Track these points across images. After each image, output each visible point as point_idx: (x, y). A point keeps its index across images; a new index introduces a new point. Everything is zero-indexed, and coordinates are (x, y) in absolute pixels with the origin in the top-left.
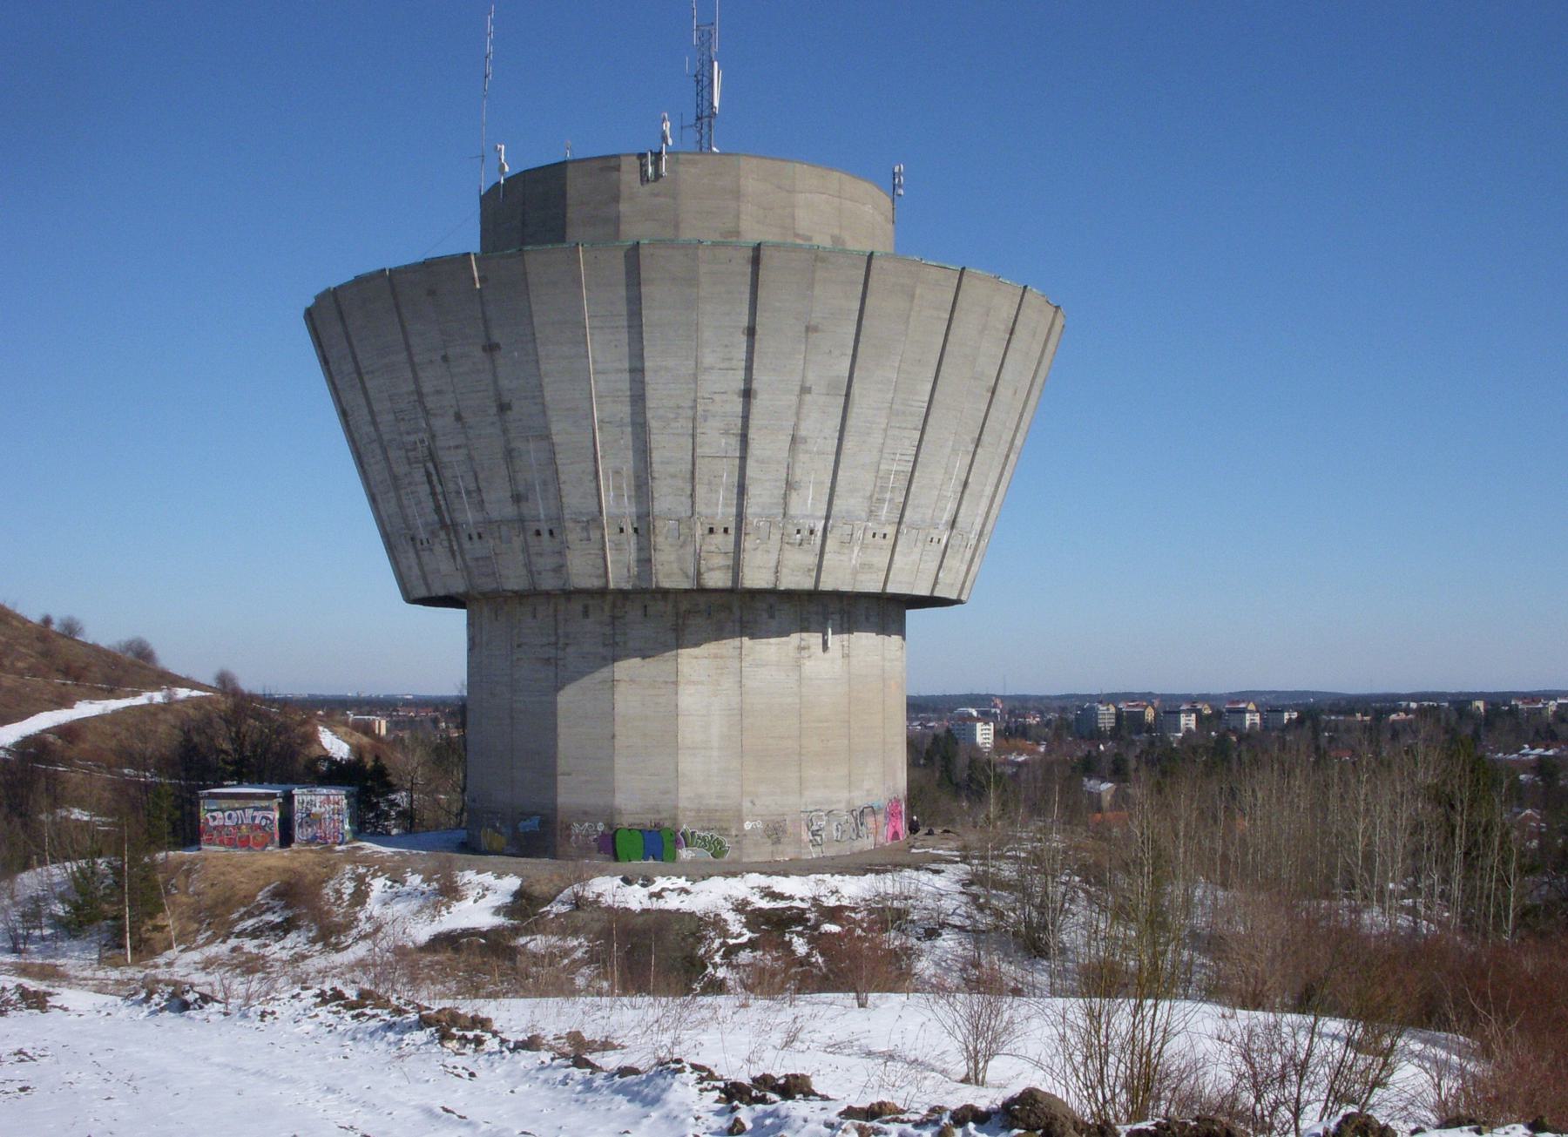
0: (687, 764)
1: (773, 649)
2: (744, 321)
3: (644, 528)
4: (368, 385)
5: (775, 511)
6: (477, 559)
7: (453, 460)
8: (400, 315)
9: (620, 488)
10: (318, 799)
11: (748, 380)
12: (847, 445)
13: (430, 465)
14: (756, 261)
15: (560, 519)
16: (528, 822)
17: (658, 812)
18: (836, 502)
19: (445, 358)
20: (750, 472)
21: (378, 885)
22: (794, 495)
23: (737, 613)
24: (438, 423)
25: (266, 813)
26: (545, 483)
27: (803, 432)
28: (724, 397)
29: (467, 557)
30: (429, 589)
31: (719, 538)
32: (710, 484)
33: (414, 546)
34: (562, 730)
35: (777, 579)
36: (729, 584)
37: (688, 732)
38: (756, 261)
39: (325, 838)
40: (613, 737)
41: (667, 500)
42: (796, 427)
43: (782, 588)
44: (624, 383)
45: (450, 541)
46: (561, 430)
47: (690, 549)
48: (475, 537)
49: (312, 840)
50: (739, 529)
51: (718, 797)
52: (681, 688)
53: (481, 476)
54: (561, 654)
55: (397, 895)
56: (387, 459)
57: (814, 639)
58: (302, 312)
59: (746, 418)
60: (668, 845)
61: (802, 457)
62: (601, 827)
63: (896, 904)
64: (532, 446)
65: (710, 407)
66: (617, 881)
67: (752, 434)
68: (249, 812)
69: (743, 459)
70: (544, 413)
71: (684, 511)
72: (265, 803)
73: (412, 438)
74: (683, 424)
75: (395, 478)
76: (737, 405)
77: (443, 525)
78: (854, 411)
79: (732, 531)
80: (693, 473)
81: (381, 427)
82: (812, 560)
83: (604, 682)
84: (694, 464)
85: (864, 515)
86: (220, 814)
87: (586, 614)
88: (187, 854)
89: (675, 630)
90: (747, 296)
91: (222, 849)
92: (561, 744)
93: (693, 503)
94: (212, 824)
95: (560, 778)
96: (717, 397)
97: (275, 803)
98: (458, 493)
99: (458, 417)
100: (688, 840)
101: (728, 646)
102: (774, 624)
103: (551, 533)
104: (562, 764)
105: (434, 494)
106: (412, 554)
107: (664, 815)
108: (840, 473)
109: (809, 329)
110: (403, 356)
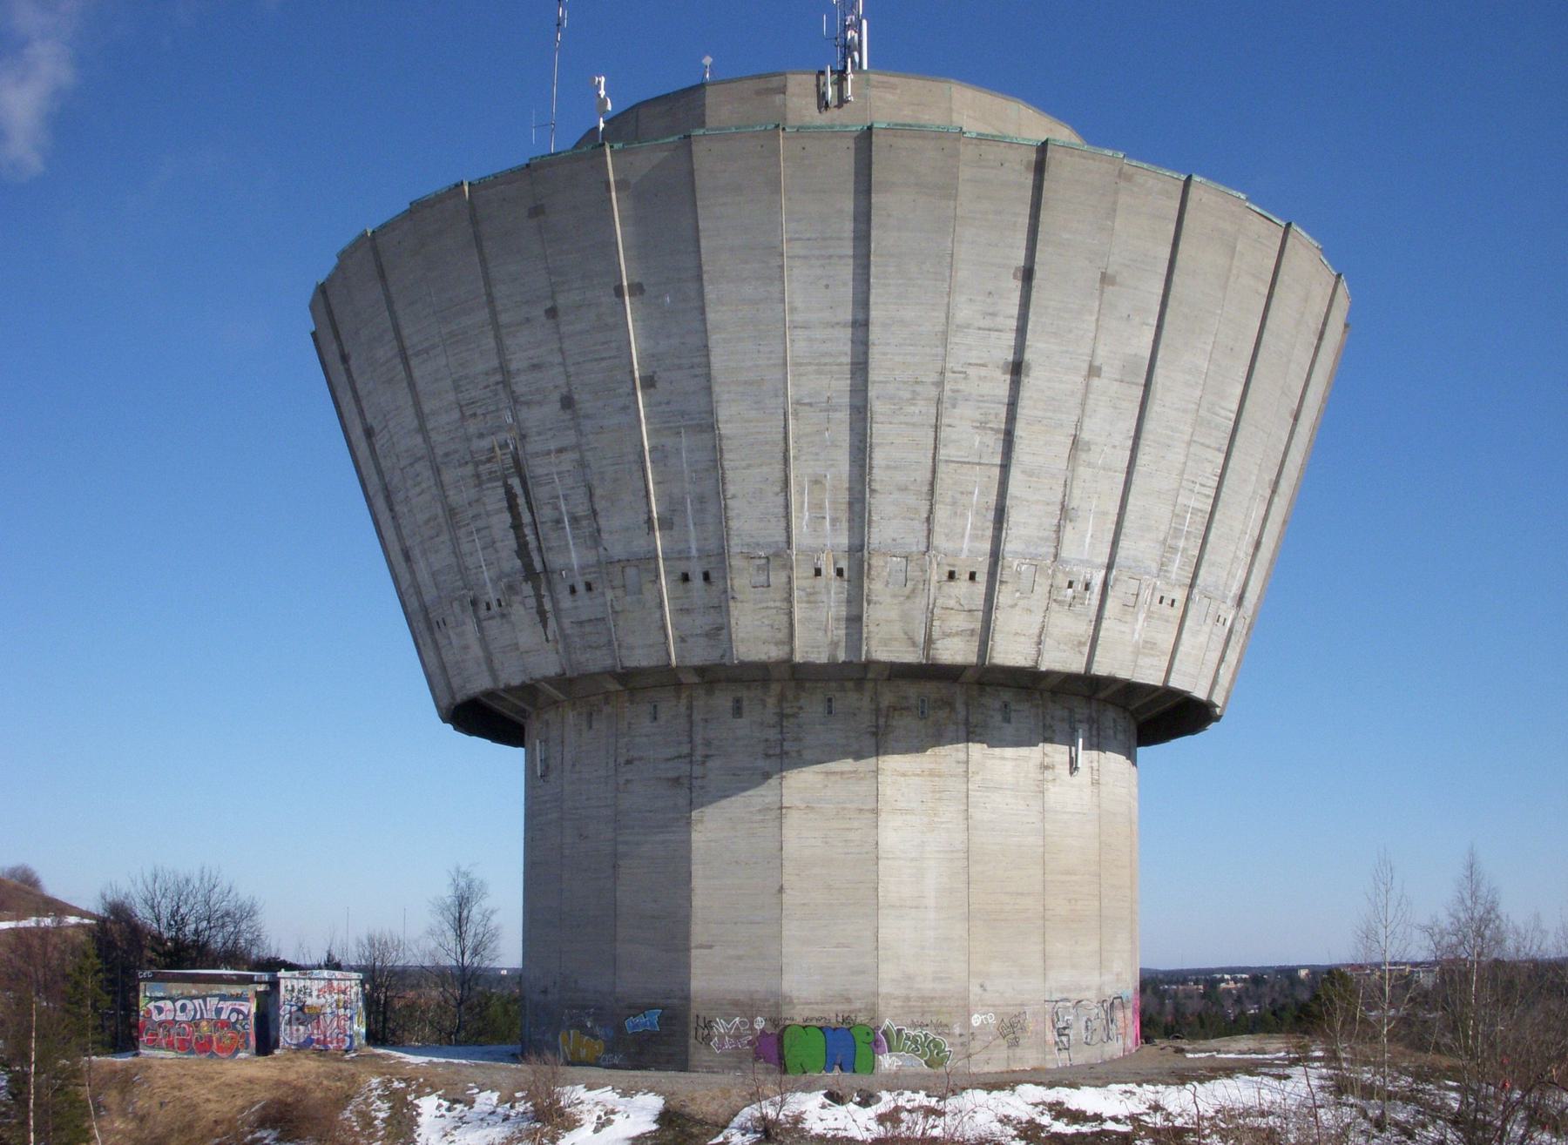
0: (890, 928)
1: (1009, 765)
2: (1019, 258)
3: (856, 567)
4: (416, 374)
5: (1043, 550)
6: (581, 623)
7: (553, 475)
8: (481, 252)
9: (821, 507)
10: (315, 986)
11: (1020, 347)
12: (1142, 459)
13: (515, 482)
14: (1040, 168)
15: (722, 555)
16: (640, 1019)
17: (848, 1000)
18: (1123, 543)
19: (552, 313)
20: (1013, 489)
21: (429, 1106)
22: (1069, 526)
23: (960, 707)
24: (532, 417)
25: (238, 1005)
26: (701, 499)
27: (1085, 436)
28: (983, 372)
29: (566, 622)
30: (495, 678)
31: (961, 586)
32: (954, 503)
33: (475, 611)
34: (698, 882)
35: (1039, 653)
36: (973, 659)
37: (894, 883)
38: (1040, 168)
39: (324, 1043)
40: (781, 890)
41: (891, 525)
42: (1079, 425)
43: (1043, 668)
44: (841, 344)
45: (539, 597)
46: (733, 416)
47: (921, 602)
48: (581, 588)
49: (304, 1046)
50: (992, 575)
51: (934, 979)
52: (883, 816)
53: (598, 492)
54: (698, 770)
55: (462, 1120)
56: (440, 484)
57: (1058, 753)
58: (308, 292)
59: (1012, 405)
60: (862, 1049)
61: (1083, 471)
62: (760, 1024)
63: (1261, 1122)
64: (684, 441)
65: (962, 386)
66: (819, 1097)
67: (1020, 430)
68: (213, 1002)
69: (1005, 467)
70: (709, 390)
71: (915, 542)
72: (236, 990)
73: (485, 443)
74: (923, 410)
75: (451, 512)
76: (1000, 386)
77: (530, 573)
78: (1154, 408)
79: (982, 578)
80: (932, 484)
81: (434, 436)
82: (1085, 629)
83: (765, 810)
84: (934, 472)
85: (1154, 567)
86: (168, 1004)
87: (738, 711)
88: (120, 1061)
89: (875, 734)
90: (1025, 221)
91: (171, 1054)
92: (698, 902)
93: (930, 532)
94: (156, 1017)
95: (694, 952)
96: (972, 371)
97: (250, 990)
98: (559, 521)
99: (567, 402)
100: (892, 1040)
101: (947, 756)
102: (1009, 729)
103: (706, 577)
104: (698, 933)
105: (517, 526)
106: (470, 627)
107: (858, 1005)
108: (1131, 500)
109: (1106, 279)
110: (484, 314)
